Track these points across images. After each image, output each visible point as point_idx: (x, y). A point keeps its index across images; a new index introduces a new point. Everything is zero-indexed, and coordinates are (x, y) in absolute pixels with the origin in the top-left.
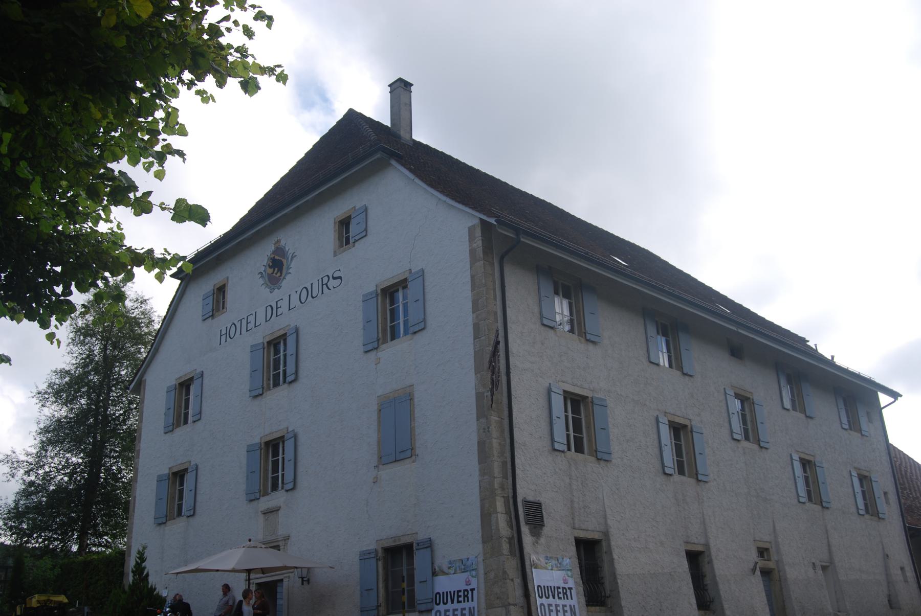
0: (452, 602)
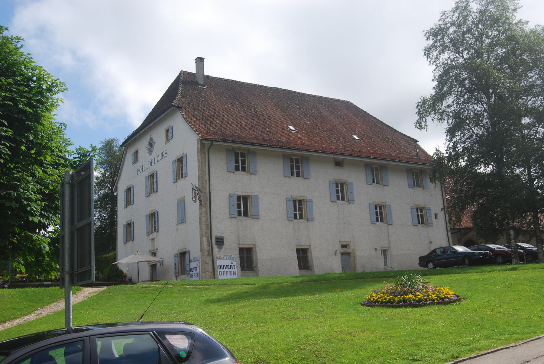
0: (226, 269)
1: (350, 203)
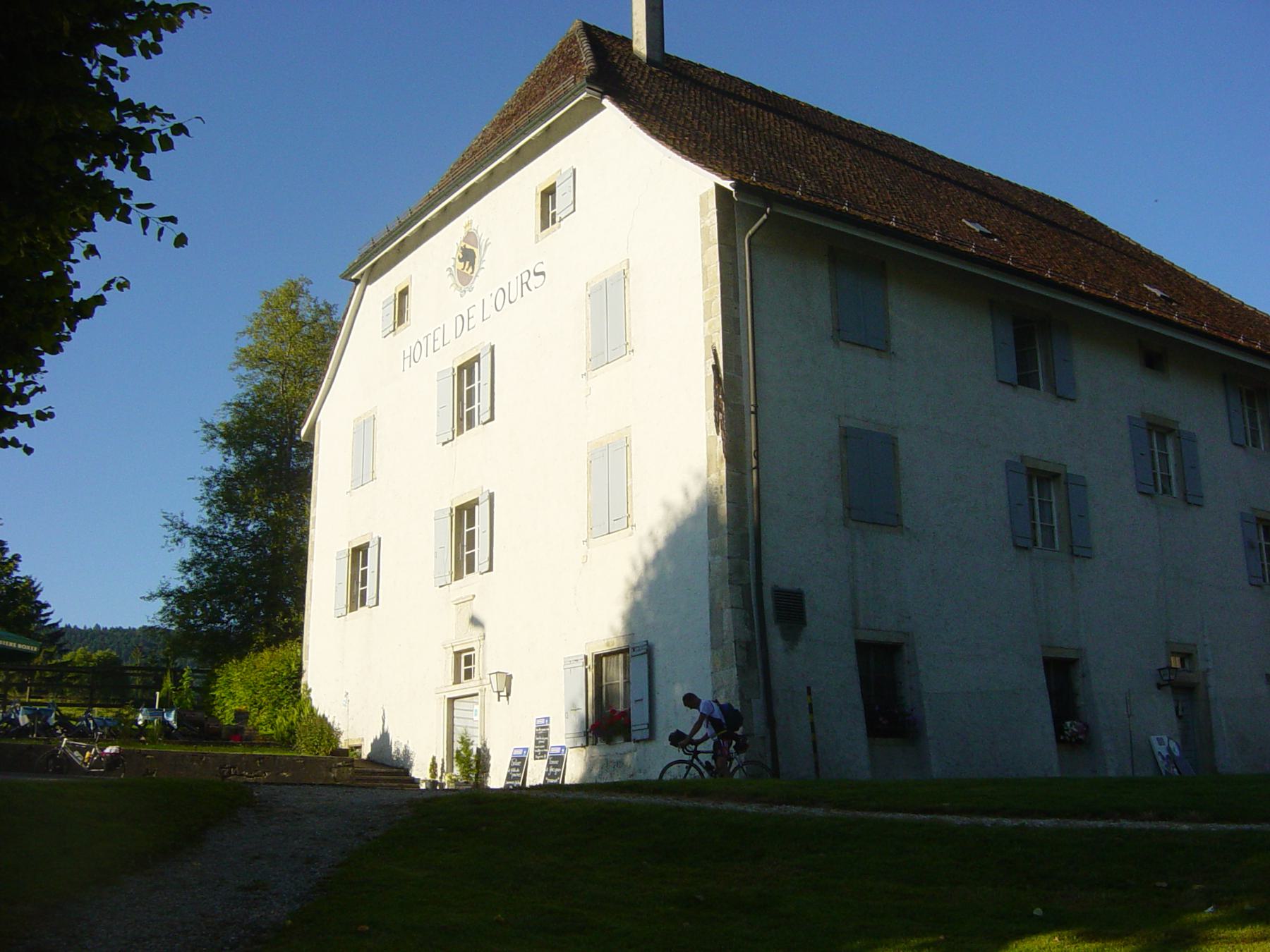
1: (1189, 503)
